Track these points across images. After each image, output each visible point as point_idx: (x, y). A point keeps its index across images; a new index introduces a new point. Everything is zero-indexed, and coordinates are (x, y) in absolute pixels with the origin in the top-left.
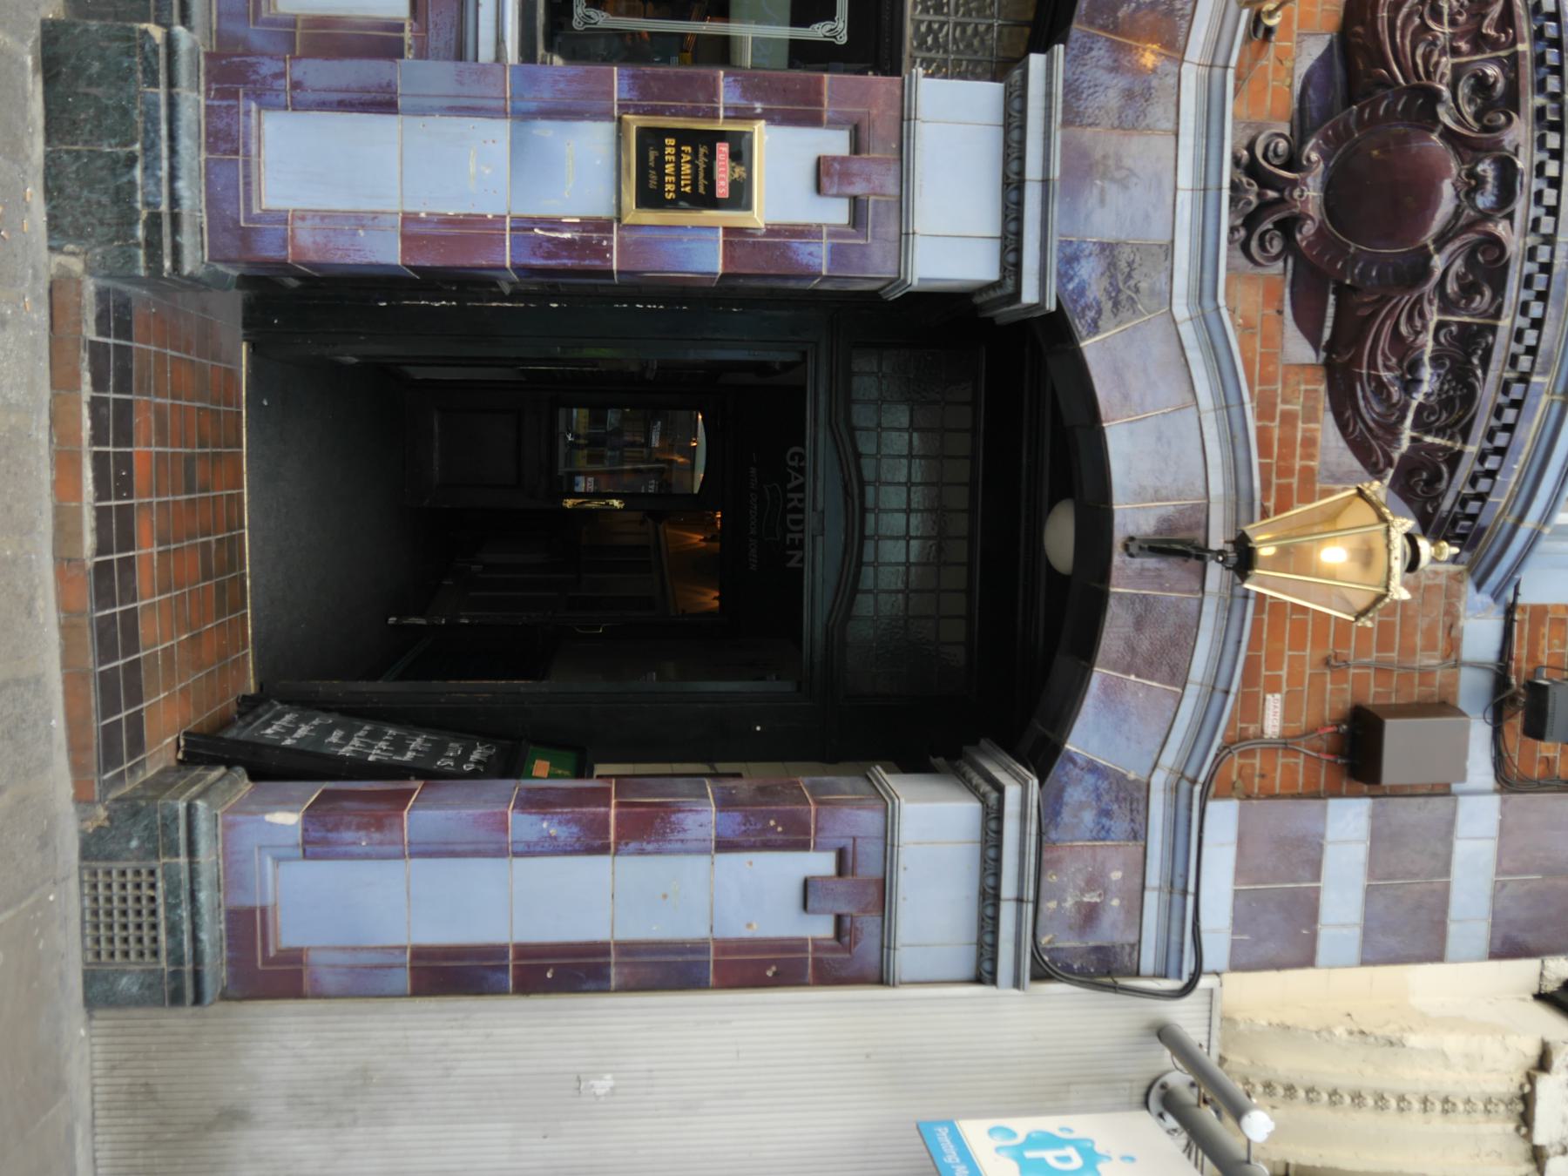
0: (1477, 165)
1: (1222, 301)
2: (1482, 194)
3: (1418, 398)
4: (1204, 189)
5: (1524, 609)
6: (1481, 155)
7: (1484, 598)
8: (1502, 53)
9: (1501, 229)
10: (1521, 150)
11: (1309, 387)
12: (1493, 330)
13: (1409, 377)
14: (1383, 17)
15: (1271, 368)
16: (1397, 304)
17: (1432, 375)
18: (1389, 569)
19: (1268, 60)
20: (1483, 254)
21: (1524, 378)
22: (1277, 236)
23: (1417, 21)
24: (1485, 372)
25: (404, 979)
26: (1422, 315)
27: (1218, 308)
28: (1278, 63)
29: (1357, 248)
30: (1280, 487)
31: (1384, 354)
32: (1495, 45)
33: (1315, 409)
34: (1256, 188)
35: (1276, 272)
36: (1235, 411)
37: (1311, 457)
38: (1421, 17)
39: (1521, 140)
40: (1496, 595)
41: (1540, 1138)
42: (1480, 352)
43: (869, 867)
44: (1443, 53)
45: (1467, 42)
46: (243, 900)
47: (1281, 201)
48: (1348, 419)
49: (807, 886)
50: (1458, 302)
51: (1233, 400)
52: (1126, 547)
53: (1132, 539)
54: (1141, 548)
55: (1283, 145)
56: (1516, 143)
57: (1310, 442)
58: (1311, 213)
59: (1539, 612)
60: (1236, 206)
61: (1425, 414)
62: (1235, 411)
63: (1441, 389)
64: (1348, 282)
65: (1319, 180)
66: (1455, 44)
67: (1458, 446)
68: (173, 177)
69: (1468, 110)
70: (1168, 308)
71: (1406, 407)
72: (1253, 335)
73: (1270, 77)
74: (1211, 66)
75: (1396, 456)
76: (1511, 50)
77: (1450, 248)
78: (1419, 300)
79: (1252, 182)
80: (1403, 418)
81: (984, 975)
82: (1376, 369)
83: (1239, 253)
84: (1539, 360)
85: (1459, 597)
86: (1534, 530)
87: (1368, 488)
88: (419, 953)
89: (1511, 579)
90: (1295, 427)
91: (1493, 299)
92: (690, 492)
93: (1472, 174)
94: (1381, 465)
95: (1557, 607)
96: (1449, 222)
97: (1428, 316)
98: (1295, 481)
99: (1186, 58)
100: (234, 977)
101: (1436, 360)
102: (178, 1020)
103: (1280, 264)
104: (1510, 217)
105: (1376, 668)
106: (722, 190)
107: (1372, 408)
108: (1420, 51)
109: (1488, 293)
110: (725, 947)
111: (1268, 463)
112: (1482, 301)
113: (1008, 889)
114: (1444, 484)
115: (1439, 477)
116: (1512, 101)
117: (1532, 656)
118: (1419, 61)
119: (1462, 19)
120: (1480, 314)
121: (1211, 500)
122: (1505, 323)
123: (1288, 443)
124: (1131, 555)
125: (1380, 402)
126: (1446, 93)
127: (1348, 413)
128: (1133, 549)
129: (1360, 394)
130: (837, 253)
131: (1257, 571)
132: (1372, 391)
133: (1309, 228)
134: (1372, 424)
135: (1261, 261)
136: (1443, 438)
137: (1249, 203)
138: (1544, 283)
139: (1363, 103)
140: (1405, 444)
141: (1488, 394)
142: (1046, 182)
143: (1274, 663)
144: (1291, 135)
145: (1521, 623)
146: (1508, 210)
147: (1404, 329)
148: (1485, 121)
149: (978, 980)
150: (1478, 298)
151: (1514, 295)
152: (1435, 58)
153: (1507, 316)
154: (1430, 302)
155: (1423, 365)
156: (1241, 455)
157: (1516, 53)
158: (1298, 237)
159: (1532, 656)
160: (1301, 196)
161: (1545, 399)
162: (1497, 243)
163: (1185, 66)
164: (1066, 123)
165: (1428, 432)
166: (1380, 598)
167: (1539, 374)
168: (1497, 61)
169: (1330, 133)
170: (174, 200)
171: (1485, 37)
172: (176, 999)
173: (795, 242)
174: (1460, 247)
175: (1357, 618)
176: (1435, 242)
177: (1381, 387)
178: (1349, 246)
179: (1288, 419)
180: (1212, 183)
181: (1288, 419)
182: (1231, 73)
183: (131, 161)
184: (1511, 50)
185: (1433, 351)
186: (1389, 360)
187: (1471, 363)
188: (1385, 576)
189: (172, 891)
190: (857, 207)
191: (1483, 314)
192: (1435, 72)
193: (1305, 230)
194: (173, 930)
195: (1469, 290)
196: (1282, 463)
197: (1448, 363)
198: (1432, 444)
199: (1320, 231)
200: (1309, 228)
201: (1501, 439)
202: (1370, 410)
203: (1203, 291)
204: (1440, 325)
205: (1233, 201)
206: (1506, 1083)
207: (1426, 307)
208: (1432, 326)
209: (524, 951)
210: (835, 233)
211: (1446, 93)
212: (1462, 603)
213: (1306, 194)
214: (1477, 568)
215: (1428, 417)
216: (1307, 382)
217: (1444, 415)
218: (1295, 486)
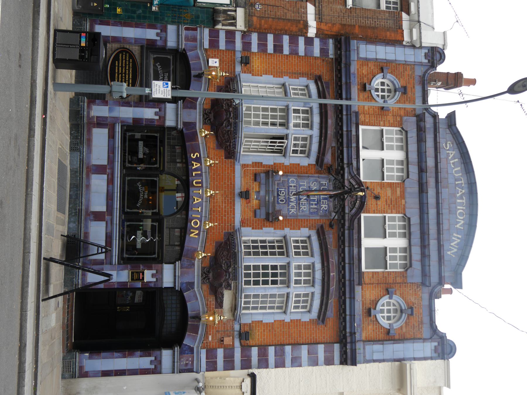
4: (198, 275)
25: (100, 374)
41: (243, 391)
43: (159, 359)
46: (81, 365)
49: (151, 361)
59: (245, 324)
68: (78, 280)
81: (173, 372)
88: (102, 371)
92: (160, 286)
100: (79, 375)
102: (73, 380)
105: (389, 329)
106: (141, 278)
110: (141, 369)
113: (176, 361)
116: (230, 266)
123: (210, 304)
130: (155, 285)
133: (211, 280)
142: (178, 276)
143: (210, 331)
149: (173, 373)
159: (244, 330)
164: (181, 268)
170: (78, 282)
172: (73, 377)
173: (150, 284)
183: (74, 278)
189: (73, 364)
190: (157, 279)
194: (73, 369)
203: (198, 287)
206: (238, 384)
209: (115, 371)
210: (154, 282)
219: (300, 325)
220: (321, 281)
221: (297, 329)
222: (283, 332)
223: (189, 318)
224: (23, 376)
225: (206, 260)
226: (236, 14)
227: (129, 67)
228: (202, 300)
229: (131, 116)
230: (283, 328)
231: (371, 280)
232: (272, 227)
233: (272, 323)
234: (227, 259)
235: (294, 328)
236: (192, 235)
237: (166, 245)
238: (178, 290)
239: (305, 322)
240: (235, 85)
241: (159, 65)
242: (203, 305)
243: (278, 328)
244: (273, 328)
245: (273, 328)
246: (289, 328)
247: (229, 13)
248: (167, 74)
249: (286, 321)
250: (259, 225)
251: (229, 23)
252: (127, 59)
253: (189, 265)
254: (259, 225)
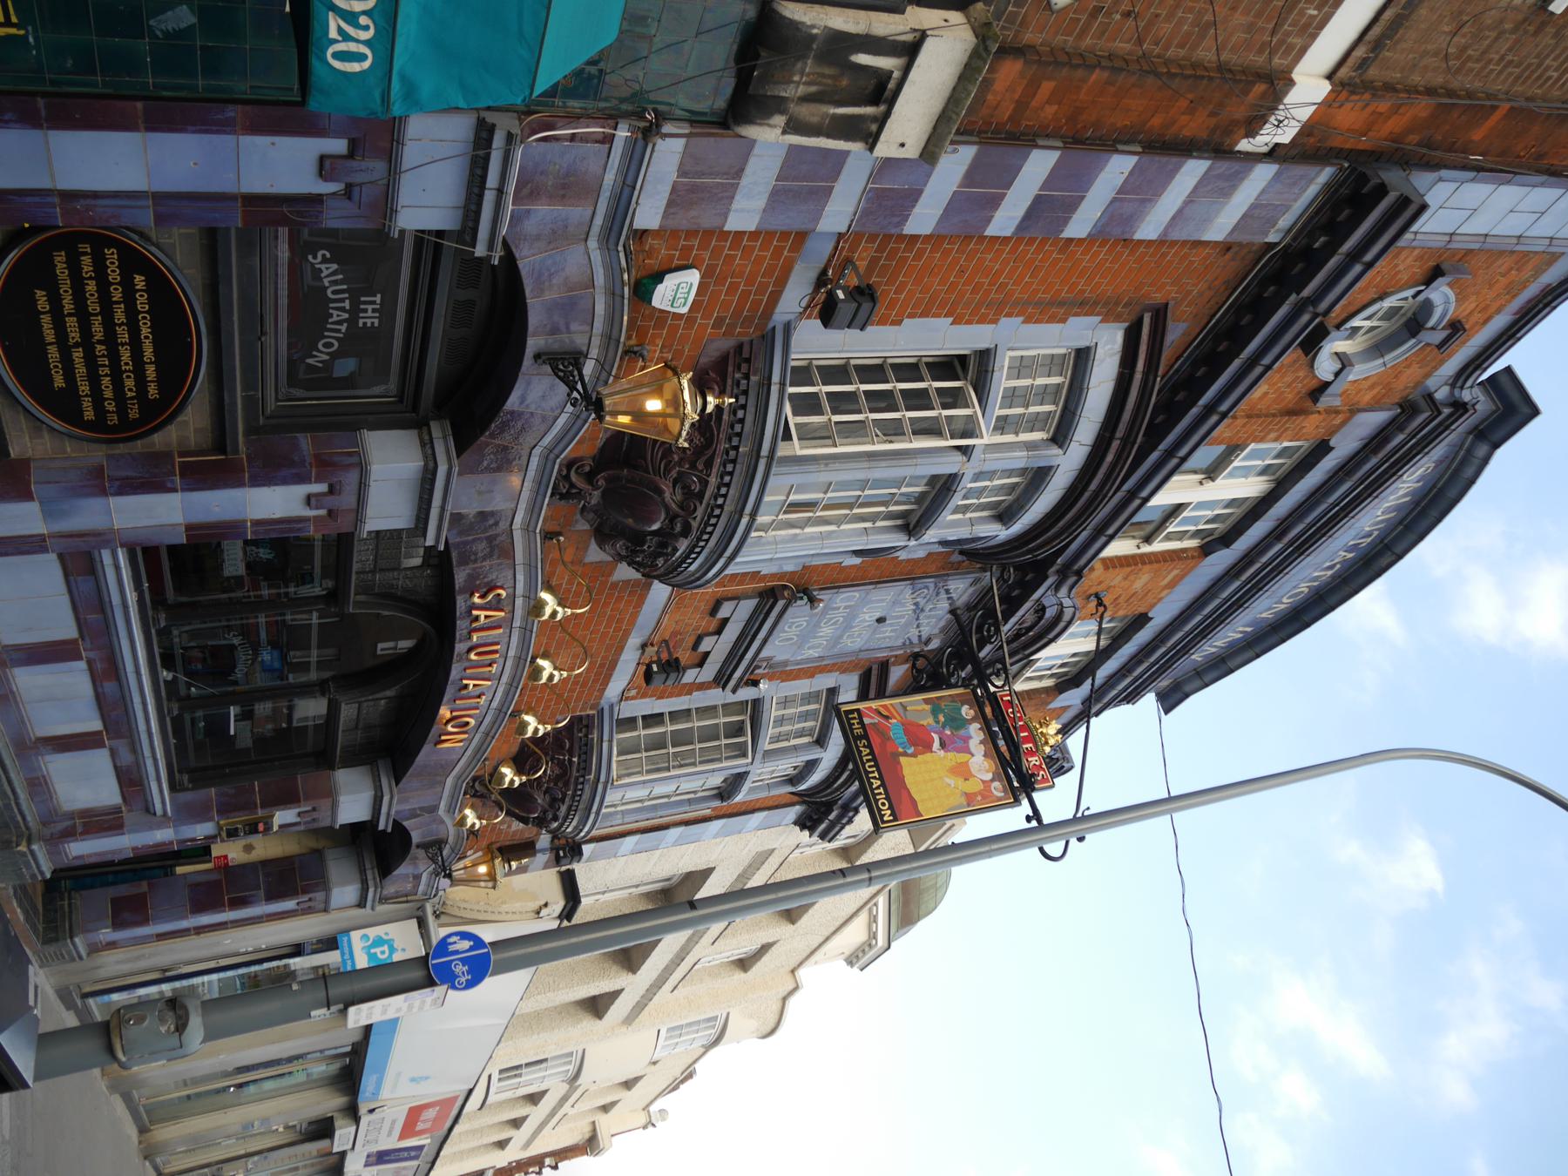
226: (489, 1168)
227: (132, 313)
229: (178, 518)
237: (357, 573)
238: (384, 831)
240: (751, 409)
241: (325, 261)
247: (863, 59)
248: (378, 298)
251: (834, 117)
252: (114, 275)
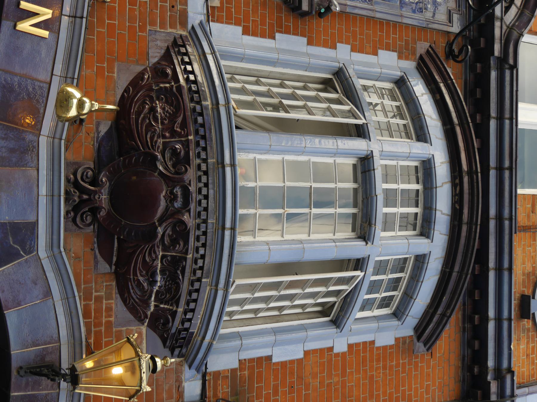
0: (174, 189)
1: (62, 249)
2: (176, 202)
3: (156, 288)
4: (52, 196)
5: (210, 374)
6: (176, 184)
7: (193, 371)
8: (183, 139)
9: (186, 217)
10: (192, 183)
11: (108, 284)
12: (185, 259)
13: (151, 279)
14: (133, 118)
15: (89, 276)
16: (143, 248)
17: (161, 278)
18: (141, 378)
19: (82, 133)
20: (178, 227)
21: (199, 280)
22: (89, 215)
23: (148, 121)
24: (183, 277)
26: (155, 252)
27: (61, 252)
28: (87, 135)
29: (125, 222)
30: (96, 332)
31: (139, 269)
32: (180, 135)
33: (111, 294)
34: (78, 193)
35: (90, 231)
36: (71, 300)
37: (110, 316)
38: (149, 119)
39: (192, 178)
40: (198, 370)
42: (180, 268)
44: (159, 137)
45: (168, 133)
47: (89, 200)
48: (126, 297)
50: (169, 247)
51: (70, 295)
52: (18, 372)
53: (21, 368)
54: (26, 372)
55: (90, 173)
56: (189, 179)
57: (109, 309)
58: (104, 206)
59: (217, 374)
60: (69, 202)
61: (160, 295)
62: (71, 300)
63: (165, 284)
64: (122, 237)
65: (107, 190)
66: (163, 133)
67: (175, 309)
69: (169, 164)
70: (36, 252)
71: (152, 292)
72: (80, 261)
73: (83, 141)
74: (54, 138)
75: (149, 313)
76: (186, 138)
77: (164, 225)
78: (153, 246)
79: (76, 191)
80: (150, 297)
82: (137, 276)
83: (71, 224)
84: (204, 272)
85: (182, 373)
86: (209, 343)
87: (132, 338)
89: (204, 362)
90: (102, 303)
91: (184, 246)
93: (172, 193)
94: (143, 317)
95: (224, 371)
96: (164, 213)
97: (158, 253)
98: (103, 328)
99: (41, 134)
101: (162, 272)
103: (92, 227)
104: (189, 211)
107: (137, 294)
108: (148, 136)
109: (182, 243)
111: (89, 321)
112: (180, 247)
114: (171, 324)
115: (169, 323)
116: (187, 161)
117: (215, 395)
118: (149, 140)
119: (166, 122)
120: (179, 252)
121: (62, 343)
122: (190, 256)
123: (98, 311)
124: (22, 376)
125: (140, 290)
126: (160, 156)
127: (126, 295)
128: (22, 372)
129: (130, 287)
131: (80, 385)
132: (136, 285)
133: (103, 213)
134: (137, 300)
135: (81, 226)
136: (168, 305)
137: (75, 201)
138: (204, 240)
139: (125, 157)
140: (152, 308)
141: (185, 287)
144: (94, 168)
145: (210, 380)
146: (188, 209)
147: (147, 259)
148: (176, 169)
150: (178, 246)
151: (193, 244)
152: (155, 139)
153: (191, 253)
154: (158, 247)
155: (157, 274)
156: (75, 321)
157: (188, 139)
158: (98, 216)
159: (215, 395)
160: (99, 198)
161: (208, 288)
162: (183, 223)
163: (41, 138)
165: (161, 303)
166: (138, 391)
167: (205, 278)
168: (181, 142)
169: (107, 173)
171: (176, 131)
174: (169, 224)
175: (130, 399)
176: (158, 221)
177: (139, 284)
178: (122, 221)
179: (98, 299)
180: (56, 193)
181: (98, 299)
182: (63, 142)
184: (186, 138)
185: (160, 268)
186: (142, 272)
187: (177, 273)
188: (139, 382)
191: (181, 252)
192: (155, 145)
193: (101, 213)
195: (174, 242)
196: (96, 321)
197: (167, 273)
198: (164, 308)
199: (108, 213)
200: (103, 213)
201: (192, 306)
202: (135, 293)
203: (52, 245)
204: (163, 257)
205: (67, 200)
207: (156, 249)
208: (160, 257)
211: (160, 156)
212: (183, 375)
213: (101, 197)
214: (188, 359)
215: (161, 296)
216: (106, 281)
217: (168, 296)
218: (103, 331)
219: (371, 361)
220: (449, 218)
221: (365, 371)
222: (329, 385)
223: (14, 373)
224: (69, 110)
225: (83, 133)
228: (68, 298)
230: (330, 376)
231: (529, 216)
232: (303, 35)
233: (299, 361)
234: (174, 134)
235: (358, 372)
236: (25, 26)
239: (385, 348)
242: (71, 314)
243: (315, 376)
244: (300, 378)
245: (300, 378)
246: (344, 374)
249: (336, 350)
250: (263, 23)
253: (12, 151)
254: (263, 23)
